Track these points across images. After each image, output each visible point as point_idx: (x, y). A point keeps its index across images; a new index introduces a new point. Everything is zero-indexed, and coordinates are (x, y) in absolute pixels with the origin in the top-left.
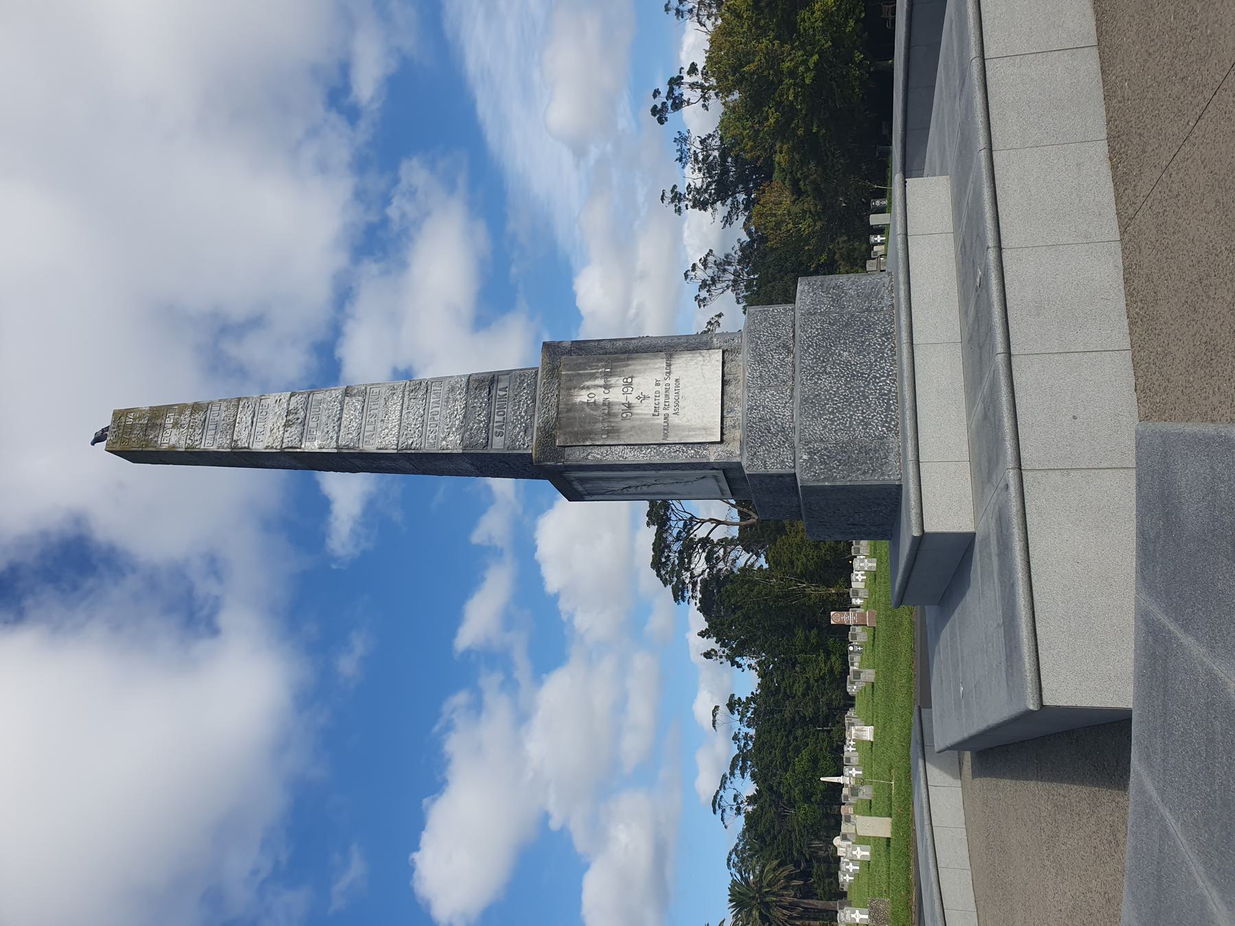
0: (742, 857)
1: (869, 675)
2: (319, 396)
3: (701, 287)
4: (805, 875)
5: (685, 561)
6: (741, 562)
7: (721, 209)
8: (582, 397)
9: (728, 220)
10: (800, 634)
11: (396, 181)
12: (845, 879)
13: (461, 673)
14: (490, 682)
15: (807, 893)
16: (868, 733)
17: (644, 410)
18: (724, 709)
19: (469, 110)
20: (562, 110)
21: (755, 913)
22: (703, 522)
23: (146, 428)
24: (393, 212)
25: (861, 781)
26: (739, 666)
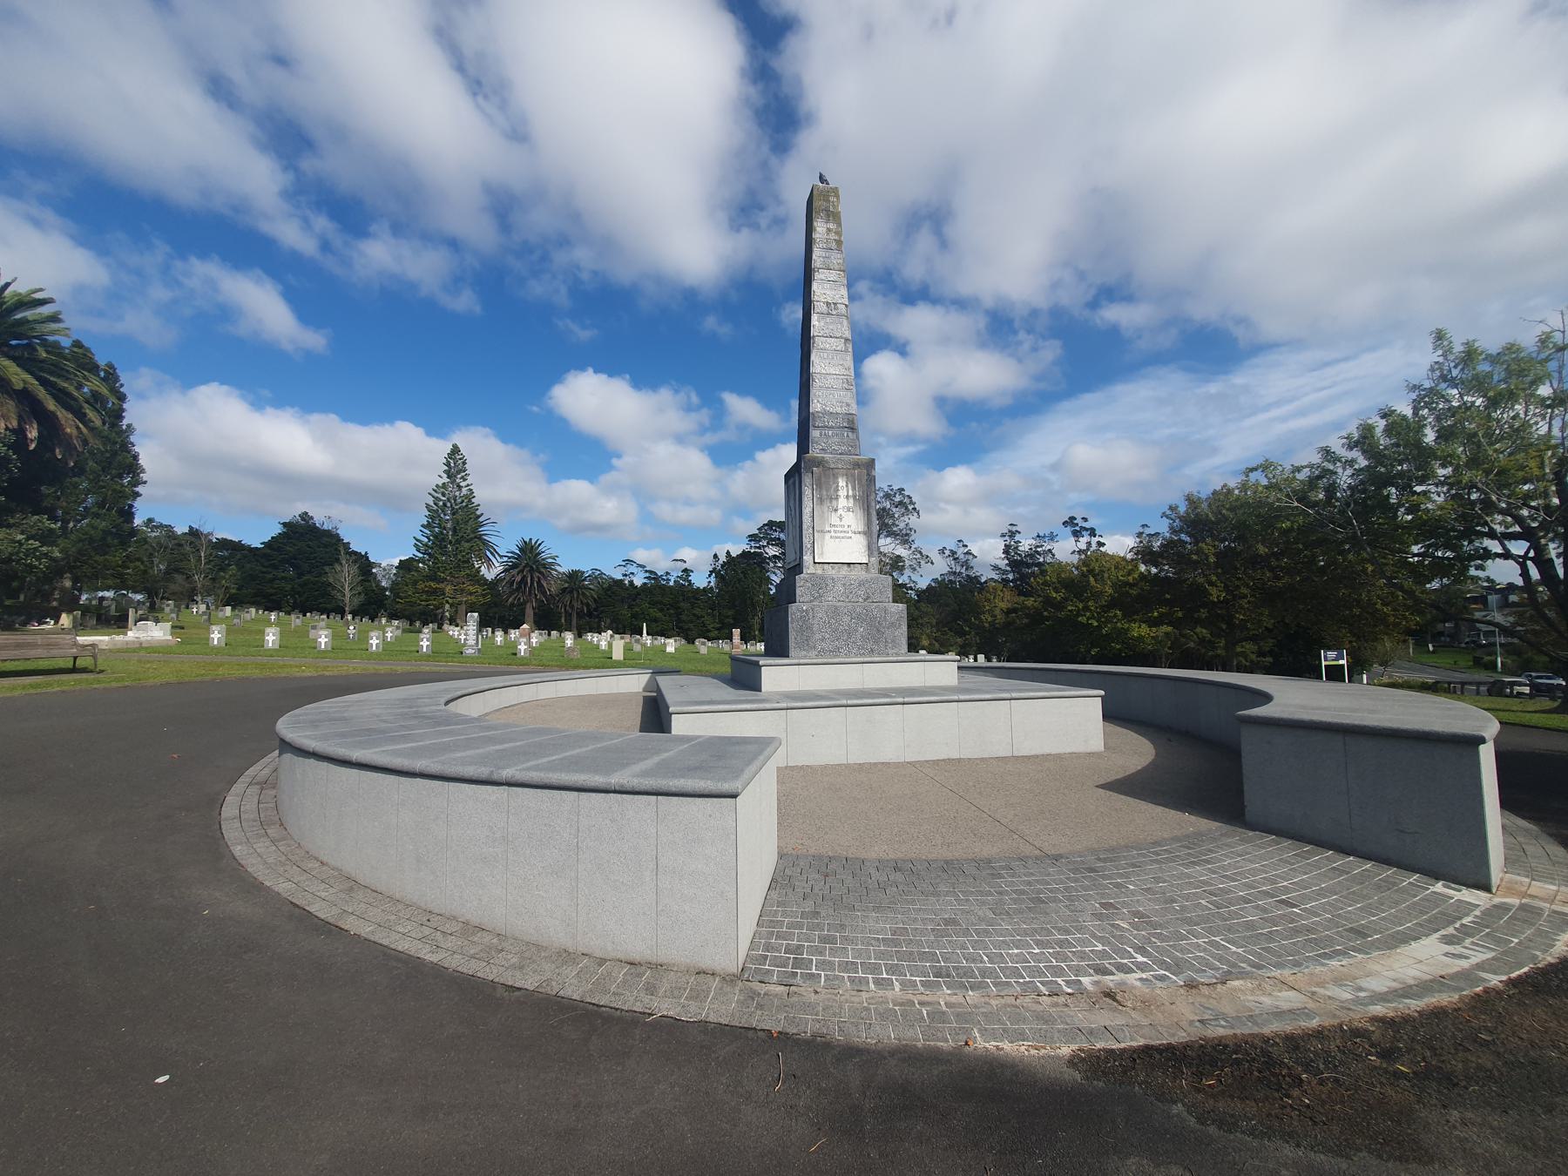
0: (597, 577)
1: (703, 650)
2: (845, 322)
4: (590, 614)
5: (771, 541)
6: (773, 577)
7: (1003, 563)
8: (842, 482)
9: (996, 568)
10: (730, 613)
11: (1044, 338)
12: (589, 636)
13: (710, 400)
14: (704, 416)
15: (580, 615)
16: (670, 649)
17: (834, 519)
18: (685, 566)
19: (1087, 388)
20: (1085, 454)
23: (827, 210)
24: (1022, 335)
25: (644, 645)
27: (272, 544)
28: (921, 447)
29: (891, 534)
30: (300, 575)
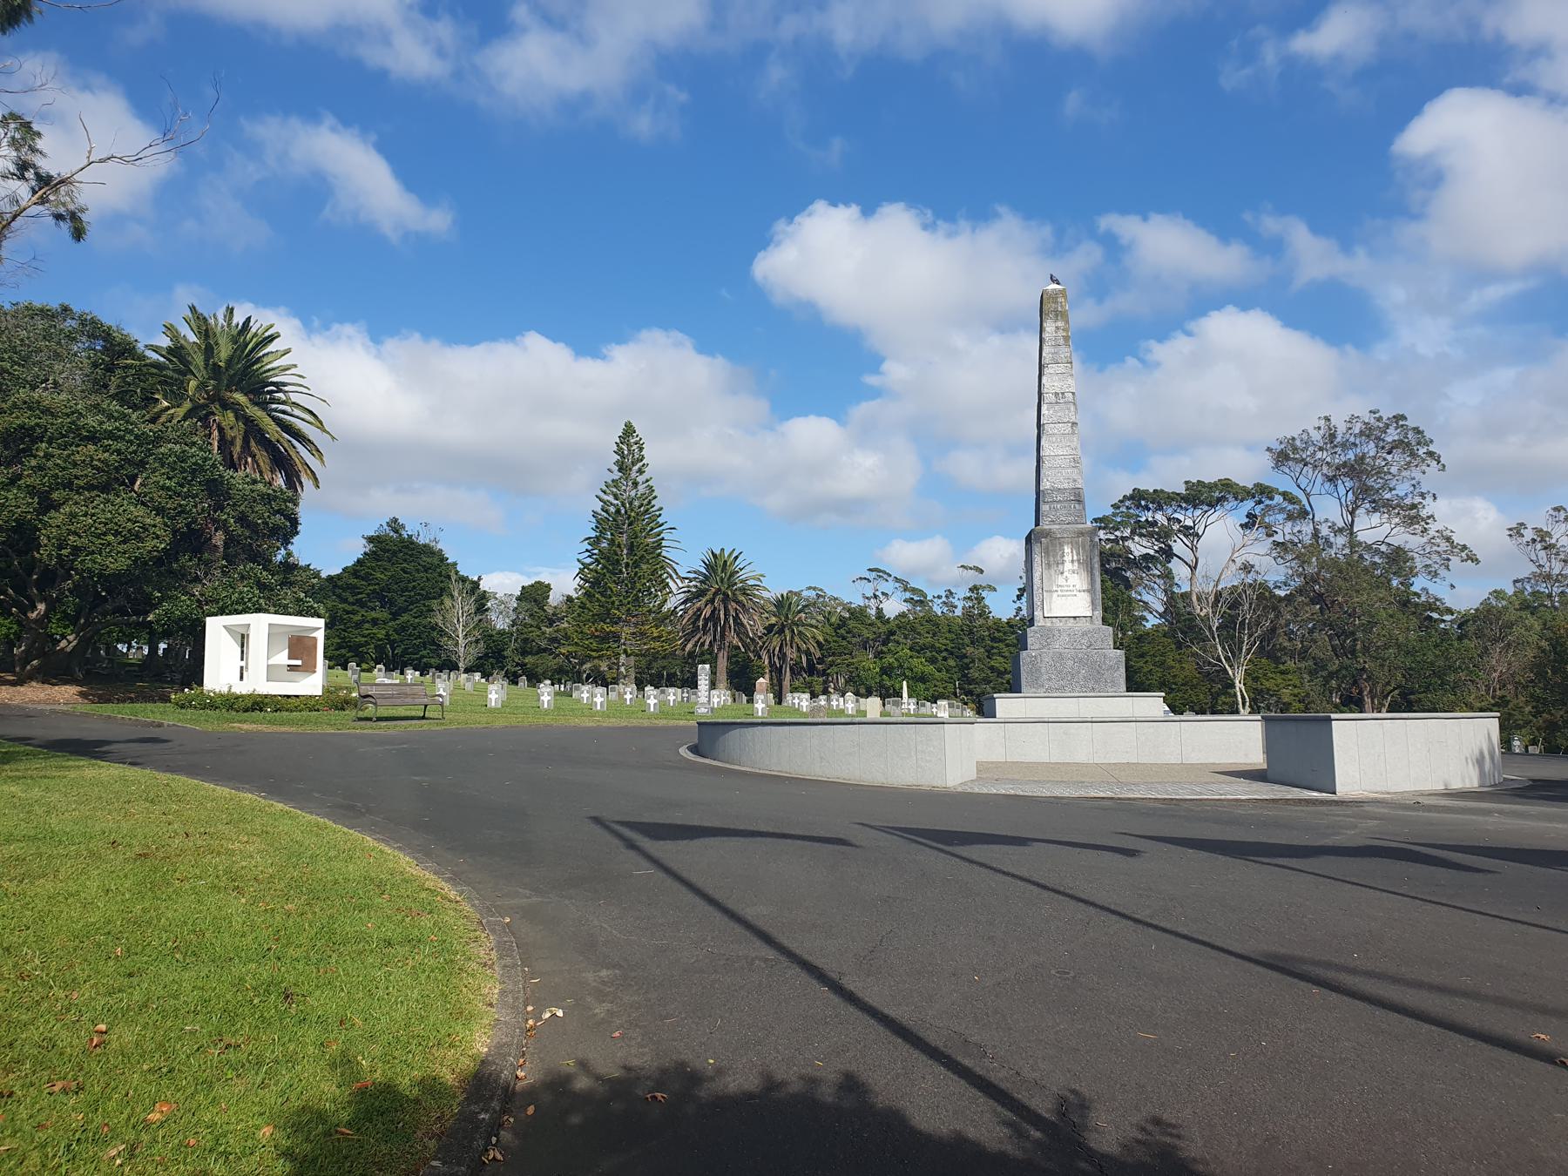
0: (818, 603)
3: (1538, 531)
5: (1139, 528)
8: (1067, 549)
17: (1061, 580)
18: (980, 580)
21: (773, 620)
22: (1193, 549)
26: (1019, 597)
27: (357, 570)
28: (1515, 287)
29: (1378, 506)
30: (395, 616)
